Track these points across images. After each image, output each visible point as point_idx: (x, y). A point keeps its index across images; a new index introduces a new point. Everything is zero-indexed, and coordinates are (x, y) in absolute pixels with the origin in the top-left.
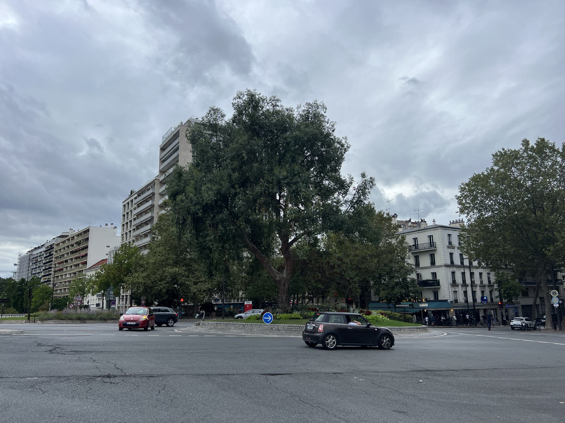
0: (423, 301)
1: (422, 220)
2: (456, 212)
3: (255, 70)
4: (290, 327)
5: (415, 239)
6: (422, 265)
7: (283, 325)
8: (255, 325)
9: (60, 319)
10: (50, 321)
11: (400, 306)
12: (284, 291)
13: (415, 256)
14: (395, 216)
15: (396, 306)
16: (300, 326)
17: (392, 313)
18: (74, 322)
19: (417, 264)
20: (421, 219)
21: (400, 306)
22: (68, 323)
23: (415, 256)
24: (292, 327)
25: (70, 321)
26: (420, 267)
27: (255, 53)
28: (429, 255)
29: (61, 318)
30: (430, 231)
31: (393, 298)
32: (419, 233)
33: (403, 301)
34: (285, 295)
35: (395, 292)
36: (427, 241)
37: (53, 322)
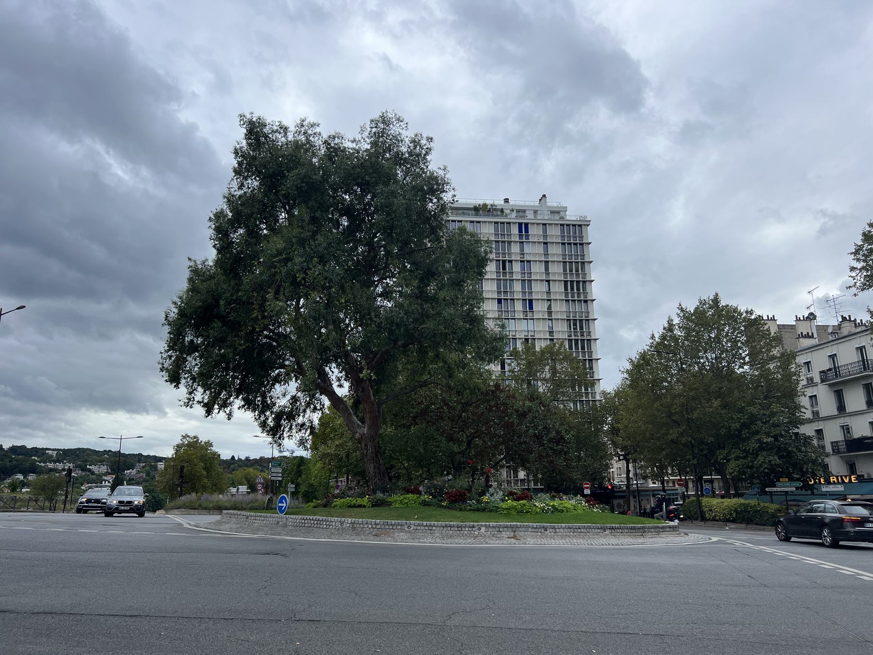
0: (853, 481)
1: (844, 319)
2: (847, 288)
3: (650, 99)
4: (303, 521)
5: (833, 357)
6: (849, 408)
7: (295, 516)
8: (260, 516)
9: (191, 508)
10: (176, 511)
11: (775, 489)
12: (369, 457)
13: (835, 391)
14: (811, 317)
15: (767, 489)
16: (319, 520)
17: (759, 504)
18: (211, 513)
19: (841, 408)
20: (842, 316)
21: (775, 489)
22: (201, 513)
23: (835, 391)
24: (306, 521)
25: (204, 512)
26: (847, 412)
27: (647, 72)
28: (862, 388)
29: (192, 506)
30: (859, 339)
31: (756, 475)
32: (839, 345)
33: (781, 480)
34: (372, 465)
35: (758, 462)
36: (855, 357)
37: (179, 511)
